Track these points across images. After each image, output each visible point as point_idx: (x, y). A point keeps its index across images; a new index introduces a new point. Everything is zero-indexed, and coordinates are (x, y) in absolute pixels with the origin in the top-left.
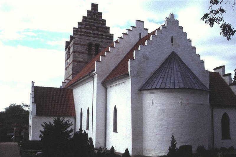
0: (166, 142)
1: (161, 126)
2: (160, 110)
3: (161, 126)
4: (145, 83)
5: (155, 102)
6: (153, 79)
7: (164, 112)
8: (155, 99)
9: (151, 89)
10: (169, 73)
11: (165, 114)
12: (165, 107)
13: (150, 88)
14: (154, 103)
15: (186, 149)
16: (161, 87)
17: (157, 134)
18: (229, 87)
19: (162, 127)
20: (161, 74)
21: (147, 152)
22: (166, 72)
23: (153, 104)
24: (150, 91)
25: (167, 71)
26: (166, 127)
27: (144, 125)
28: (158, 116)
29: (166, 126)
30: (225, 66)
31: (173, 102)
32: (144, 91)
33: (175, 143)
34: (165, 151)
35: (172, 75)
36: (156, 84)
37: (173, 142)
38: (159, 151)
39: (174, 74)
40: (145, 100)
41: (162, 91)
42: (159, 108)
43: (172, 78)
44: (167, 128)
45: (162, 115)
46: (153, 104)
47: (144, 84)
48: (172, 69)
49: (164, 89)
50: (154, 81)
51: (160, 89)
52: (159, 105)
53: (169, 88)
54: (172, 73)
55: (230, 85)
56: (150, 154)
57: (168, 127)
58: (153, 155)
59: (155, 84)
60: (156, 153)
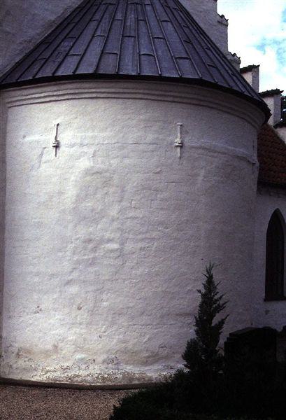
0: (110, 317)
1: (90, 246)
2: (88, 172)
3: (90, 246)
4: (21, 57)
5: (65, 138)
6: (58, 42)
7: (107, 183)
8: (69, 124)
9: (54, 80)
10: (128, 24)
11: (111, 190)
12: (114, 162)
13: (47, 72)
14: (62, 143)
15: (256, 340)
16: (101, 72)
17: (69, 283)
18: (273, 131)
19: (94, 250)
20: (93, 25)
21: (21, 363)
22: (93, 37)
23: (57, 146)
24: (49, 90)
25: (119, 16)
26: (117, 250)
27: (7, 242)
28: (79, 199)
29: (115, 246)
30: (260, 68)
31: (150, 137)
32: (19, 93)
33: (215, 321)
34: (104, 357)
35: (143, 29)
36: (77, 59)
37: (209, 306)
38: (79, 356)
39: (148, 28)
40: (22, 133)
41: (104, 88)
42: (85, 163)
43: (142, 41)
44: (115, 255)
45: (99, 196)
46: (57, 146)
47: (19, 64)
48: (139, 10)
49: (117, 78)
50: (62, 49)
51: (95, 77)
52: (85, 149)
53: (139, 78)
54: (141, 23)
55: (276, 126)
56: (35, 369)
57: (121, 250)
58: (48, 374)
59: (69, 59)
60: (66, 365)
